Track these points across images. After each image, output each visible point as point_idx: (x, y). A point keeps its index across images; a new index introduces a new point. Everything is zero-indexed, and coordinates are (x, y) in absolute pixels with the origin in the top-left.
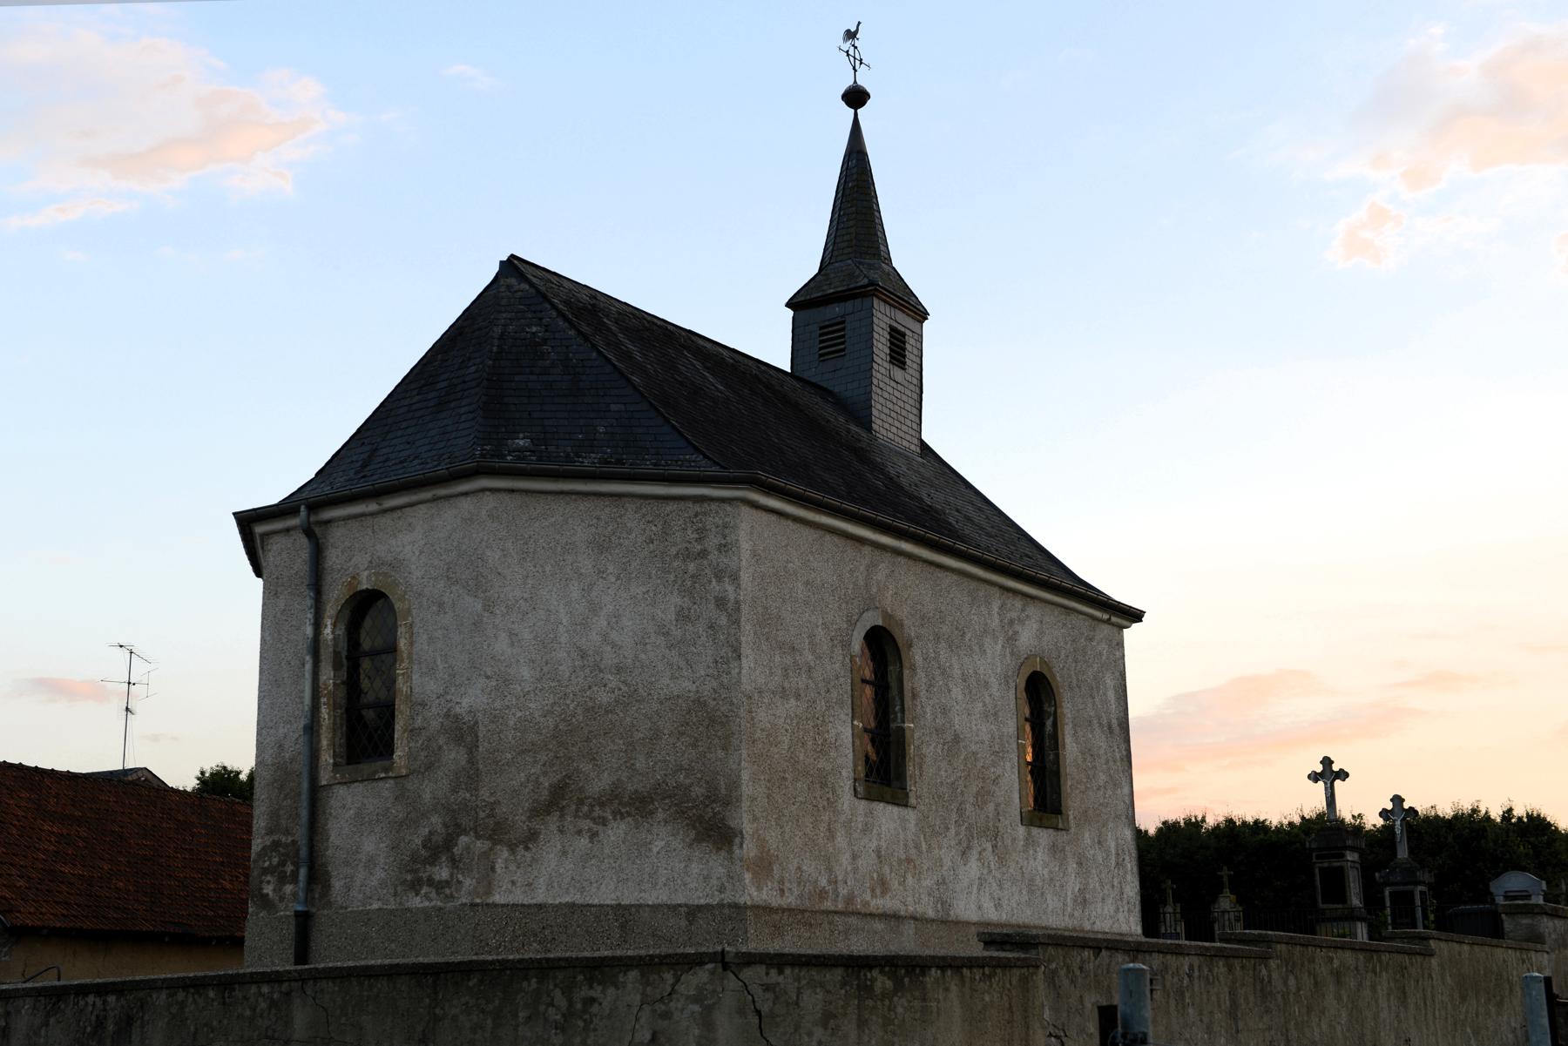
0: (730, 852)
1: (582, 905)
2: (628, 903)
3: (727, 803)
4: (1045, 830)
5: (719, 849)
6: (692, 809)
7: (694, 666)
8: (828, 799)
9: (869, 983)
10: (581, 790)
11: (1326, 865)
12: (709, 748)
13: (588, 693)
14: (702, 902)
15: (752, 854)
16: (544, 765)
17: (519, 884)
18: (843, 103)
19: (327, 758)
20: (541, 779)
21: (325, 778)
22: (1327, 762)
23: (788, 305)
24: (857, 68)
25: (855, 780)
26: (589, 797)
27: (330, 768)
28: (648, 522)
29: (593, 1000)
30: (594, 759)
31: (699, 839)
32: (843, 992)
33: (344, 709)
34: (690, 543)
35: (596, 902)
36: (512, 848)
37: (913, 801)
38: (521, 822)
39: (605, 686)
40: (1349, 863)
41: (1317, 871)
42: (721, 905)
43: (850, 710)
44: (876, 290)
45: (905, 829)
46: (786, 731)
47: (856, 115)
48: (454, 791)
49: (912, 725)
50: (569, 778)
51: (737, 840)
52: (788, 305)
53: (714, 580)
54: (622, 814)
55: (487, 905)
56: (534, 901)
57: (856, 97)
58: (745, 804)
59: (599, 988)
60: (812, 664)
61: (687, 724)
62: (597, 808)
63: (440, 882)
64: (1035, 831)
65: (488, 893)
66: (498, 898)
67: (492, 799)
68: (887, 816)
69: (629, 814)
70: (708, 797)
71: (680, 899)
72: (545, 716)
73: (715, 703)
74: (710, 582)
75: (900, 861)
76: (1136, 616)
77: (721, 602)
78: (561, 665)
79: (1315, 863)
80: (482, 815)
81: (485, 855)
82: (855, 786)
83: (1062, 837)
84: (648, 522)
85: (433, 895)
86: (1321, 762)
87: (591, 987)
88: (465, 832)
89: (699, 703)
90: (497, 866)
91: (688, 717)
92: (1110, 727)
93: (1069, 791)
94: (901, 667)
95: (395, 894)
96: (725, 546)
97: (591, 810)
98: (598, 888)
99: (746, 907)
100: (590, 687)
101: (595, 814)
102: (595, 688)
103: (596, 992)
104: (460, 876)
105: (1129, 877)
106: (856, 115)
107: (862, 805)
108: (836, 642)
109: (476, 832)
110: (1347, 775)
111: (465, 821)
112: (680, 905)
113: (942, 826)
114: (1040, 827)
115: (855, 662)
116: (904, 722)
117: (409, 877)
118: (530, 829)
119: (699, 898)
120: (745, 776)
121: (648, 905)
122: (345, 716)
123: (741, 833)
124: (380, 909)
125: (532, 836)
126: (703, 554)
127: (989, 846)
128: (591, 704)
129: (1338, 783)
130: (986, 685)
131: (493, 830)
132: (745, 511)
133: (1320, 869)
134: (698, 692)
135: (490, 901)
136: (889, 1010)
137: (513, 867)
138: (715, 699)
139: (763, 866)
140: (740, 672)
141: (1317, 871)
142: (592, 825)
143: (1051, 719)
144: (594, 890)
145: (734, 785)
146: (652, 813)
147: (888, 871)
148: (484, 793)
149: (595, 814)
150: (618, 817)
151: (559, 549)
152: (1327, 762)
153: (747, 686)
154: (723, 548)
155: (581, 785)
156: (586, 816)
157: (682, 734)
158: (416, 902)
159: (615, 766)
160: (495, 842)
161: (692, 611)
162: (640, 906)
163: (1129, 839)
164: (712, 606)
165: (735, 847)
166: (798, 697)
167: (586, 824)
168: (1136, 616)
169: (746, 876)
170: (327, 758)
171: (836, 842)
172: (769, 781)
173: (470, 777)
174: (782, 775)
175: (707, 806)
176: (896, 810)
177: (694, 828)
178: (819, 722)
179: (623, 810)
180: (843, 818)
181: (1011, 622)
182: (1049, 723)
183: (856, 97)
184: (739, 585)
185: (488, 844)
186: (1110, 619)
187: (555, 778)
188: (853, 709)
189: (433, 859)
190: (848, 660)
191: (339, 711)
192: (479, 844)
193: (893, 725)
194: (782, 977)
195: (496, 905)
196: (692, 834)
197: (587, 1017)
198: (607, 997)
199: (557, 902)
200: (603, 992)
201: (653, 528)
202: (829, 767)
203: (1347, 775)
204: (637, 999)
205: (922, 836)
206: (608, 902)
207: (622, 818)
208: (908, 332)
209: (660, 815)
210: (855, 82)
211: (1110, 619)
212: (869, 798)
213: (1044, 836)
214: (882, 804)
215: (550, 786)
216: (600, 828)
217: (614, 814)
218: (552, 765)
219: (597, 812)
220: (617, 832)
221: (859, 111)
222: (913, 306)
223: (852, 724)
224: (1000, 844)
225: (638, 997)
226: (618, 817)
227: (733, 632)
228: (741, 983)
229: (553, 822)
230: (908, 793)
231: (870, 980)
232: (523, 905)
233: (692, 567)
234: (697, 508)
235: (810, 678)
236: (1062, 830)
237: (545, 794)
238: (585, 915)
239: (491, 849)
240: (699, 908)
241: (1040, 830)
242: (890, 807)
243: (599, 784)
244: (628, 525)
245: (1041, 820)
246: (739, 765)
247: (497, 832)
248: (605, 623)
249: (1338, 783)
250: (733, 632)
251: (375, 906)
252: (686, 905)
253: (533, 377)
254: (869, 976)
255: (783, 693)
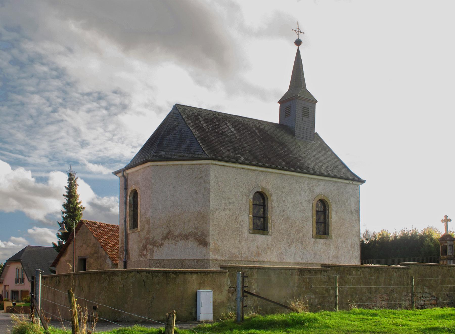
0: (207, 247)
1: (173, 260)
2: (183, 259)
3: (206, 236)
4: (322, 239)
5: (204, 247)
6: (198, 238)
7: (199, 204)
8: (240, 234)
9: (169, 276)
10: (173, 234)
11: (442, 245)
12: (202, 223)
13: (174, 212)
14: (200, 259)
15: (212, 248)
16: (165, 228)
17: (159, 255)
18: (295, 44)
19: (128, 228)
20: (164, 232)
21: (129, 232)
22: (446, 217)
23: (278, 102)
24: (299, 34)
25: (249, 229)
26: (175, 235)
27: (129, 229)
28: (189, 170)
29: (113, 279)
30: (176, 227)
31: (199, 244)
32: (163, 277)
33: (132, 216)
34: (199, 175)
35: (176, 259)
36: (158, 247)
37: (270, 233)
38: (160, 241)
39: (178, 210)
40: (448, 245)
41: (440, 247)
42: (204, 259)
43: (248, 212)
44: (297, 97)
45: (267, 241)
46: (225, 218)
47: (298, 48)
48: (147, 235)
49: (271, 215)
50: (170, 231)
51: (208, 245)
52: (278, 102)
53: (204, 183)
54: (182, 239)
55: (152, 259)
56: (162, 259)
57: (298, 43)
58: (211, 236)
59: (114, 276)
60: (235, 202)
61: (197, 218)
62: (176, 238)
63: (145, 255)
64: (318, 240)
65: (153, 257)
66: (154, 258)
67: (153, 236)
68: (260, 238)
69: (184, 239)
70: (202, 235)
71: (195, 258)
72: (165, 217)
73: (204, 213)
74: (203, 184)
75: (265, 249)
76: (363, 182)
77: (205, 189)
78: (168, 205)
79: (440, 245)
80: (151, 240)
81: (152, 249)
82: (249, 230)
83: (328, 241)
84: (189, 170)
85: (144, 258)
86: (444, 217)
87: (113, 276)
88: (148, 244)
89: (200, 213)
90: (154, 251)
91: (197, 216)
92: (351, 212)
93: (333, 229)
94: (268, 201)
95: (139, 257)
96: (207, 175)
97: (175, 238)
98: (177, 256)
99: (210, 260)
100: (175, 210)
101: (176, 239)
102: (176, 210)
103: (114, 277)
104: (148, 253)
105: (356, 251)
106: (298, 48)
107: (252, 236)
108: (243, 196)
109: (150, 244)
110: (451, 220)
111: (148, 242)
112: (195, 259)
113: (282, 240)
114: (320, 239)
115: (250, 200)
116: (268, 214)
117: (140, 254)
118: (161, 243)
119: (199, 258)
120: (211, 229)
121: (188, 260)
122: (133, 218)
123: (209, 243)
124: (136, 261)
125: (162, 244)
126: (202, 177)
127: (300, 244)
128: (175, 214)
129: (448, 223)
130: (301, 203)
131: (153, 243)
132: (212, 166)
133: (441, 246)
134: (200, 210)
135: (153, 259)
136: (174, 281)
137: (158, 251)
138: (204, 212)
139: (216, 251)
140: (210, 205)
141: (440, 247)
142: (175, 242)
143: (328, 211)
144: (176, 256)
145: (208, 232)
146: (189, 239)
147: (261, 251)
148: (152, 235)
149: (176, 239)
150: (181, 240)
151: (168, 178)
152: (446, 217)
153: (212, 208)
154: (206, 175)
155: (173, 232)
156: (174, 240)
157: (196, 220)
158: (141, 259)
159: (180, 228)
160: (154, 246)
161: (199, 191)
162: (186, 260)
163: (357, 241)
164: (203, 190)
165: (208, 246)
166: (229, 210)
167: (174, 242)
168: (363, 182)
169: (210, 253)
170: (128, 228)
171: (242, 244)
172: (219, 231)
173: (149, 232)
174: (223, 229)
175: (201, 237)
176: (264, 236)
177: (198, 242)
178: (237, 216)
179: (182, 238)
180: (244, 239)
181: (312, 186)
182: (327, 212)
183: (298, 43)
184: (210, 184)
185: (152, 246)
186: (353, 183)
187: (167, 231)
188: (249, 212)
189: (143, 250)
190: (248, 200)
191: (131, 217)
192: (150, 246)
193: (266, 215)
194: (149, 274)
195: (154, 260)
196: (198, 243)
197: (112, 282)
198: (116, 278)
199: (167, 259)
200: (115, 277)
201: (190, 172)
202: (240, 226)
203: (451, 220)
204: (120, 279)
205: (274, 242)
206: (179, 259)
207: (182, 240)
208: (309, 107)
209: (191, 239)
210: (298, 38)
211: (353, 183)
212: (254, 233)
213: (321, 241)
214: (259, 235)
215: (166, 233)
216: (177, 242)
217: (180, 239)
218: (166, 228)
219: (176, 239)
220: (181, 243)
221: (299, 47)
222: (308, 99)
223: (249, 216)
224: (304, 243)
225: (121, 278)
226: (181, 240)
227: (208, 196)
228: (140, 276)
229: (166, 241)
230: (268, 232)
231: (170, 275)
232: (160, 260)
233: (199, 181)
234: (200, 166)
235: (234, 205)
236: (329, 239)
237: (165, 235)
238: (173, 262)
239: (153, 247)
240: (199, 260)
241: (320, 239)
242: (261, 236)
243: (176, 234)
244: (184, 171)
245: (320, 237)
246: (209, 227)
247: (154, 244)
248: (178, 195)
249: (448, 223)
250: (208, 196)
251: (136, 260)
252: (196, 260)
253: (172, 136)
254: (169, 274)
255: (225, 210)
